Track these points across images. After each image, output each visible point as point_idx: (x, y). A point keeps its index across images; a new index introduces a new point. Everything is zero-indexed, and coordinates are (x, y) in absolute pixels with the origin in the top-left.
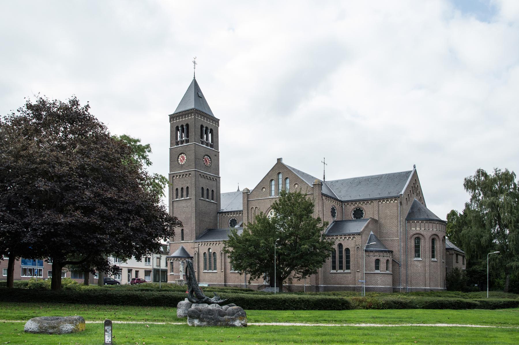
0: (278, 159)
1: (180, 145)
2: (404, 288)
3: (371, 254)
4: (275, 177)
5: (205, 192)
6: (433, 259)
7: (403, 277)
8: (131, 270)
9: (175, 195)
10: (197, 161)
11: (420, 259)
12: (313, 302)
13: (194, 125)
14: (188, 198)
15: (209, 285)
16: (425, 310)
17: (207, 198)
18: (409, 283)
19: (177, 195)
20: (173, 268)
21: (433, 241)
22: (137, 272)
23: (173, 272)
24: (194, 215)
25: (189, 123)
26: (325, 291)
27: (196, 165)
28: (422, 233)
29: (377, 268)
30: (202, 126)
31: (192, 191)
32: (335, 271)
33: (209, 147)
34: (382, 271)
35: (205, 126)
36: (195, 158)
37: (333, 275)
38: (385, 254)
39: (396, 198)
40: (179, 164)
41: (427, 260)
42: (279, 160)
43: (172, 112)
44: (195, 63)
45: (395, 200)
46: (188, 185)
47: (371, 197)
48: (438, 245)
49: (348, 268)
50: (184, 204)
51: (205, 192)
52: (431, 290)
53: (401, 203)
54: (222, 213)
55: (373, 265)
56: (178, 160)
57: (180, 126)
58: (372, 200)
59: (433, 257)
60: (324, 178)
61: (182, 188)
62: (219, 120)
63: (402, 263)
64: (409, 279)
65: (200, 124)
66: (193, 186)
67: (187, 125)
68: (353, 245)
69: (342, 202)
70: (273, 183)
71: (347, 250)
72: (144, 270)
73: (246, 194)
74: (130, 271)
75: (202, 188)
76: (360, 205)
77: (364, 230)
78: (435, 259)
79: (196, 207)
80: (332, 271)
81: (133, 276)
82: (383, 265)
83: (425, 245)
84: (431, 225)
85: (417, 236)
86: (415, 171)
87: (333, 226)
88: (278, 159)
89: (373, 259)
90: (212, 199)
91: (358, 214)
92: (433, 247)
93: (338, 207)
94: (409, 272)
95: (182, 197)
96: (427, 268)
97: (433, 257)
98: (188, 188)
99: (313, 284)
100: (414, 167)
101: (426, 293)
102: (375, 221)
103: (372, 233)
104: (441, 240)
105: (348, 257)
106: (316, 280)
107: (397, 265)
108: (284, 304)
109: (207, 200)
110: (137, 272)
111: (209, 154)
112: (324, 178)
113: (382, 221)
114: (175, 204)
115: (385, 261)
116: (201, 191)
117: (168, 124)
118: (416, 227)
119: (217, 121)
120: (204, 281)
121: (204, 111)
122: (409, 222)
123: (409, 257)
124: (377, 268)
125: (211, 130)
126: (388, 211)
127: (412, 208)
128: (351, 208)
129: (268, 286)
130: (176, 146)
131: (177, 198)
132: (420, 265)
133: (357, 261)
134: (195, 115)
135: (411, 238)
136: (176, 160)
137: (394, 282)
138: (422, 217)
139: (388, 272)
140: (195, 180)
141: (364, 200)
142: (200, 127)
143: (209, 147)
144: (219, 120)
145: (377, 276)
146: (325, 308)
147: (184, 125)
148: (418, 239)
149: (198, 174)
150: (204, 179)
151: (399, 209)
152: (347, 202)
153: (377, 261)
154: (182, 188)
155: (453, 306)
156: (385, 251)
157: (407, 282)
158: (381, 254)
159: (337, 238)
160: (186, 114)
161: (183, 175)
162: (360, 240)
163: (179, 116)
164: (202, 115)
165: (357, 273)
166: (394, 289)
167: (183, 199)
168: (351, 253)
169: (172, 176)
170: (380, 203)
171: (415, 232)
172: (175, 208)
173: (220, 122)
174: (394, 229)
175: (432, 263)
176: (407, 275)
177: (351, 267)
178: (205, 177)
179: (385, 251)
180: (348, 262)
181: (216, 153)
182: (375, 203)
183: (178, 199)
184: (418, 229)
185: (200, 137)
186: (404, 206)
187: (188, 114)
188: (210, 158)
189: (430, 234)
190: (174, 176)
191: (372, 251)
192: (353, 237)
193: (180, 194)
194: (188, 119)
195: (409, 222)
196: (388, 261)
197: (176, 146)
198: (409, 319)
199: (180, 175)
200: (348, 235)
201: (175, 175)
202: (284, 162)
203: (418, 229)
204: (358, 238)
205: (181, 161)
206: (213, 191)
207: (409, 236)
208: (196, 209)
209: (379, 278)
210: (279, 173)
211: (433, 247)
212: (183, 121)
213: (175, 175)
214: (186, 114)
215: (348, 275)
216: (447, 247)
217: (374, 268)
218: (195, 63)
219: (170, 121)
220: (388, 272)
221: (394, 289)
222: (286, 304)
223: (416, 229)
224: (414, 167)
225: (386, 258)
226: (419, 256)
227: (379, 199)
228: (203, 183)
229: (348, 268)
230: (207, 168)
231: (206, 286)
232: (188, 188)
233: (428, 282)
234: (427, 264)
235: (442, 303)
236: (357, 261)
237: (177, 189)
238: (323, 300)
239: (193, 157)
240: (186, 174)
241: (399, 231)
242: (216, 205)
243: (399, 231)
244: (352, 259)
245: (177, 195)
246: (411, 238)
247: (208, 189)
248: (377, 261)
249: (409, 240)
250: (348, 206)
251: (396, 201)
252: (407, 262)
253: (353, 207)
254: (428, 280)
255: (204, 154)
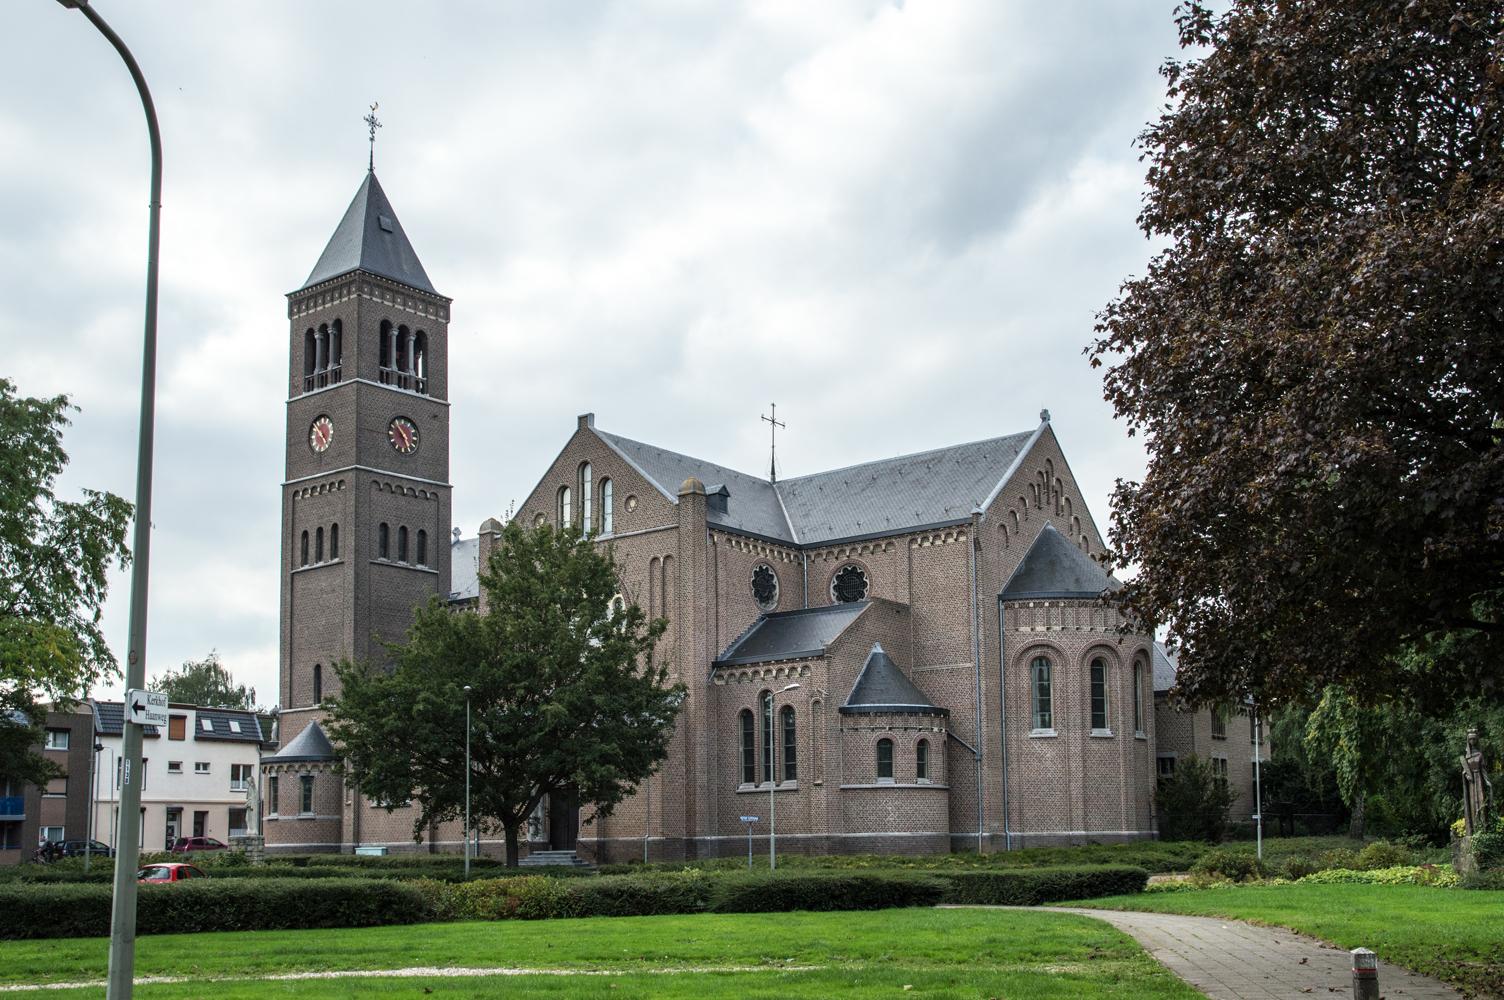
0: (581, 419)
1: (316, 391)
2: (992, 838)
3: (864, 722)
4: (570, 478)
5: (394, 538)
6: (1096, 732)
7: (988, 798)
8: (180, 810)
9: (298, 553)
10: (365, 439)
11: (1051, 732)
12: (267, 902)
13: (355, 323)
14: (336, 560)
15: (386, 851)
16: (748, 917)
17: (403, 558)
18: (1015, 816)
19: (305, 552)
20: (276, 798)
21: (1097, 668)
22: (200, 818)
23: (275, 811)
24: (350, 615)
25: (343, 318)
26: (722, 854)
27: (359, 451)
28: (1055, 641)
29: (885, 770)
30: (385, 326)
31: (347, 540)
32: (751, 787)
33: (394, 388)
34: (902, 780)
35: (396, 322)
36: (359, 429)
37: (747, 800)
38: (912, 721)
39: (961, 526)
40: (312, 449)
41: (1076, 735)
42: (585, 420)
43: (298, 284)
44: (372, 122)
45: (960, 533)
46: (335, 519)
47: (893, 526)
48: (1117, 681)
49: (791, 773)
50: (323, 582)
51: (394, 538)
52: (1092, 841)
53: (977, 543)
54: (461, 602)
55: (871, 759)
56: (310, 440)
57: (316, 328)
58: (889, 537)
59: (1098, 721)
60: (773, 473)
61: (320, 530)
62: (449, 301)
63: (985, 751)
64: (1015, 804)
65: (380, 317)
66: (351, 519)
67: (338, 324)
68: (803, 695)
69: (799, 548)
70: (568, 495)
71: (787, 711)
72: (226, 809)
73: (488, 538)
74: (174, 813)
75: (384, 526)
76: (854, 557)
77: (839, 642)
78: (1107, 732)
79: (357, 588)
80: (745, 787)
81: (187, 829)
82: (904, 759)
83: (1069, 683)
84: (1085, 612)
85: (1038, 652)
86: (1047, 434)
87: (758, 631)
88: (581, 419)
89: (868, 738)
90: (422, 560)
91: (850, 586)
92: (1097, 689)
93: (780, 565)
94: (1014, 779)
95: (319, 557)
96: (1073, 765)
97: (1098, 721)
98: (335, 526)
99: (674, 835)
100: (1045, 416)
101: (1068, 849)
102: (899, 610)
103: (878, 649)
104: (1128, 664)
105: (790, 734)
106: (688, 820)
107: (969, 756)
108: (163, 912)
109: (402, 563)
110: (200, 818)
111: (410, 415)
112: (773, 473)
113: (923, 608)
114: (299, 584)
115: (913, 746)
116: (376, 536)
117: (284, 325)
118: (1032, 623)
119: (442, 305)
120: (375, 836)
121: (398, 276)
122: (1012, 607)
123: (1013, 726)
124: (885, 770)
125: (421, 335)
126: (938, 573)
127: (1031, 558)
128: (829, 567)
129: (544, 847)
130: (305, 394)
131: (305, 562)
132: (1049, 752)
133: (815, 748)
134: (360, 289)
135: (1018, 660)
136: (305, 439)
137: (955, 815)
138: (1058, 588)
139: (923, 782)
140: (357, 500)
141: (865, 540)
142: (377, 327)
143: (394, 388)
144: (449, 301)
145: (881, 797)
146: (312, 923)
147: (330, 323)
148: (1042, 660)
149: (366, 479)
150: (389, 496)
151: (972, 562)
152: (816, 547)
153: (885, 747)
154: (320, 530)
155: (834, 897)
156: (926, 712)
157: (1006, 815)
158: (899, 722)
159: (756, 673)
160: (334, 289)
161: (323, 486)
162: (825, 678)
163: (314, 297)
164: (384, 289)
165: (814, 791)
166: (954, 840)
167: (321, 564)
168: (800, 719)
169: (292, 490)
170: (915, 546)
171: (1029, 641)
172: (297, 595)
173: (452, 306)
174: (959, 633)
175: (1095, 746)
176: (1005, 792)
177: (799, 771)
178: (393, 488)
179: (926, 712)
180: (790, 753)
181: (435, 410)
182: (900, 545)
183: (306, 567)
184: (1040, 628)
185: (377, 361)
186: (991, 554)
187: (341, 287)
188: (414, 425)
189: (1083, 645)
190: (296, 493)
191: (864, 713)
192: (805, 667)
193: (312, 551)
194: (343, 305)
195: (1012, 607)
196: (922, 745)
197: (305, 394)
198: (408, 955)
199: (314, 488)
200: (802, 659)
201: (300, 489)
202: (599, 426)
203: (1040, 628)
204: (818, 669)
205: (319, 440)
206: (422, 533)
207: (1013, 653)
208: (356, 598)
209: (891, 806)
210: (585, 464)
211: (1097, 689)
212: (324, 311)
213: (300, 489)
214: (334, 289)
215: (792, 798)
216: (1157, 688)
217: (874, 772)
218: (372, 122)
219: (291, 314)
220: (923, 782)
221: (954, 840)
222: (171, 913)
223: (1035, 627)
224: (1045, 416)
225: (916, 736)
226: (1045, 724)
227: (913, 534)
228: (387, 509)
229: (791, 773)
230: (402, 458)
231: (377, 853)
232: (335, 526)
233: (1078, 812)
234: (1076, 749)
235: (789, 891)
236: (815, 748)
237: (305, 534)
238: (605, 893)
239: (351, 426)
240: (332, 484)
241: (974, 639)
242: (432, 580)
243: (974, 639)
244: (801, 743)
245: (305, 552)
246: (1018, 660)
247: (404, 529)
248: (885, 747)
249: (1012, 669)
250: (820, 560)
251: (962, 539)
252: (1005, 744)
253: (834, 564)
254: (1080, 805)
255: (390, 415)
